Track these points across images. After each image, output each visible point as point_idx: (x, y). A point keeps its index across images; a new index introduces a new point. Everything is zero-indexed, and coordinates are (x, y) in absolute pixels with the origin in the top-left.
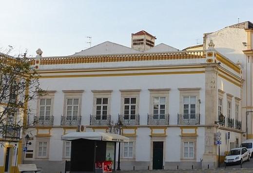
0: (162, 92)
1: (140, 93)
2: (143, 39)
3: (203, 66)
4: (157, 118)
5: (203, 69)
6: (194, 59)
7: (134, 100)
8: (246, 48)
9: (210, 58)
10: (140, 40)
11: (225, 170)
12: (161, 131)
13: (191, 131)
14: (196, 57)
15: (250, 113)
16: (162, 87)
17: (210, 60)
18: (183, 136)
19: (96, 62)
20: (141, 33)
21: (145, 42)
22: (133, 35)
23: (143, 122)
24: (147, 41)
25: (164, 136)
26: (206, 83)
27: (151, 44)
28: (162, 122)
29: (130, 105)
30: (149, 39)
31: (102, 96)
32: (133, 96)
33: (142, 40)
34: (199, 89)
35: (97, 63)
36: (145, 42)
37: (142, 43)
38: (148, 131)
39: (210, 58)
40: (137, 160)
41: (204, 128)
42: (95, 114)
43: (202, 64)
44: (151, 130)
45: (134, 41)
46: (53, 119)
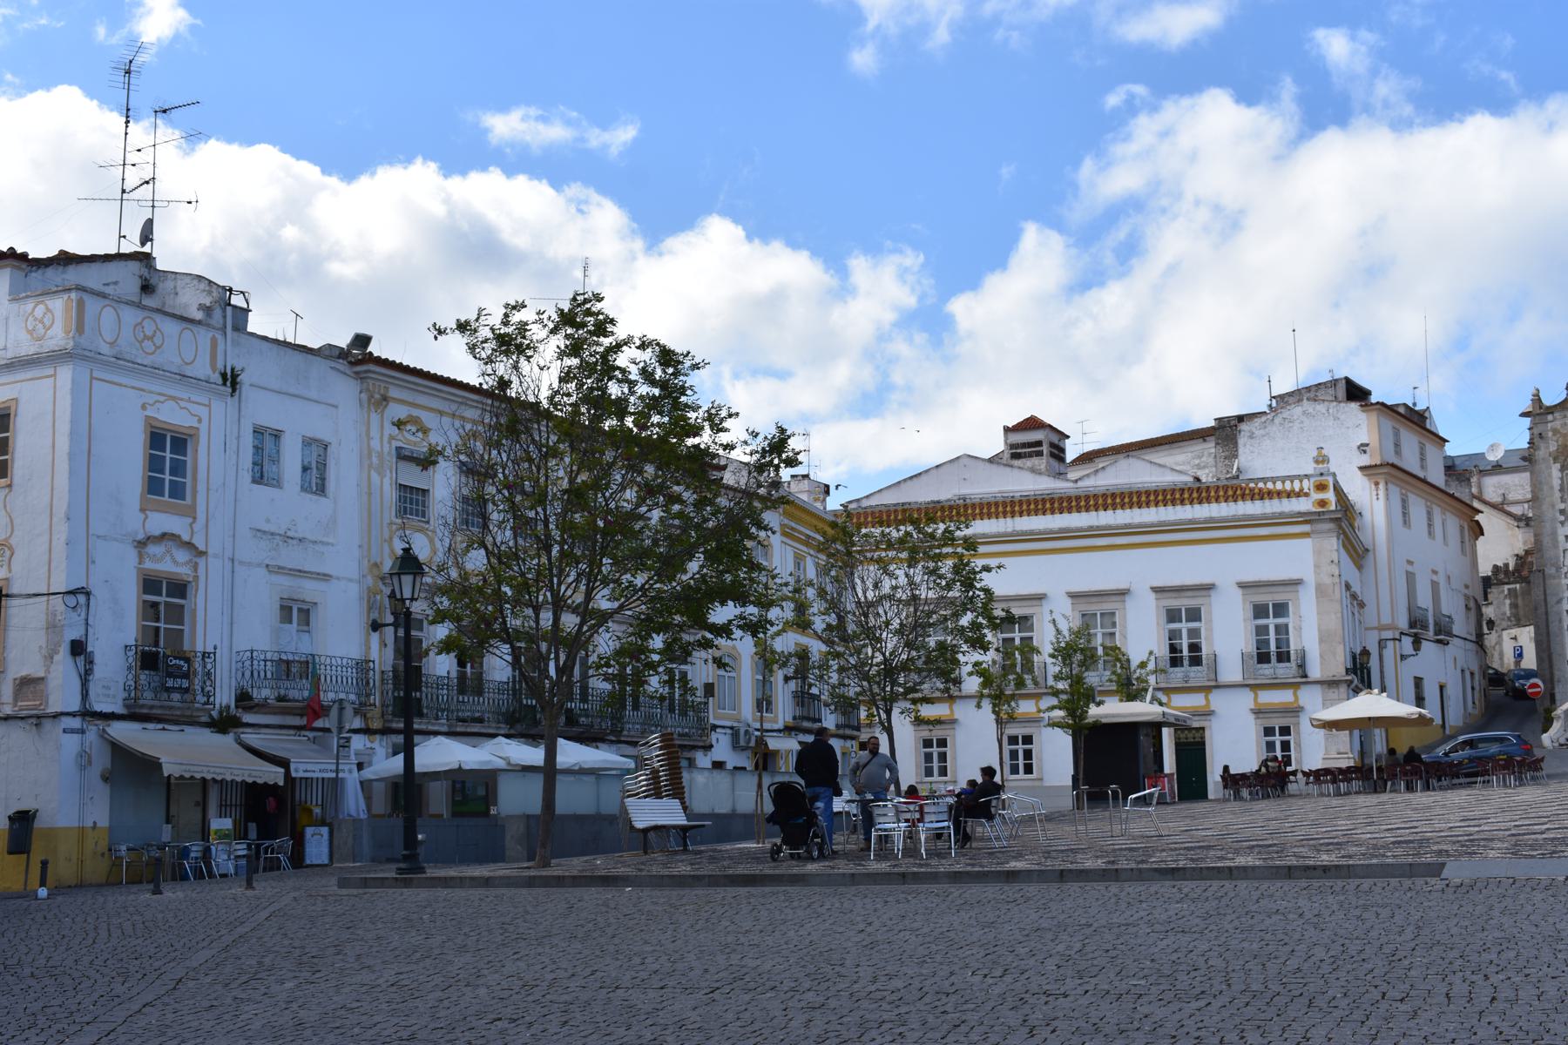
0: (1190, 594)
1: (1127, 598)
2: (1034, 441)
4: (1269, 661)
6: (1276, 501)
7: (1194, 615)
8: (1365, 460)
9: (1321, 496)
10: (1030, 445)
11: (1338, 794)
12: (1282, 697)
13: (1282, 697)
14: (1279, 494)
15: (1390, 644)
16: (1189, 581)
17: (1322, 503)
18: (1258, 712)
19: (1148, 505)
20: (1032, 424)
22: (1007, 430)
23: (1231, 671)
25: (1208, 714)
26: (1317, 566)
28: (1197, 675)
29: (935, 750)
30: (1055, 439)
31: (1183, 602)
32: (1280, 597)
33: (1039, 443)
34: (1298, 583)
35: (993, 521)
36: (1045, 449)
37: (1040, 454)
38: (1246, 700)
39: (1321, 496)
40: (1047, 783)
41: (1318, 688)
42: (1251, 648)
43: (1300, 514)
44: (1251, 695)
45: (1012, 446)
46: (1303, 658)
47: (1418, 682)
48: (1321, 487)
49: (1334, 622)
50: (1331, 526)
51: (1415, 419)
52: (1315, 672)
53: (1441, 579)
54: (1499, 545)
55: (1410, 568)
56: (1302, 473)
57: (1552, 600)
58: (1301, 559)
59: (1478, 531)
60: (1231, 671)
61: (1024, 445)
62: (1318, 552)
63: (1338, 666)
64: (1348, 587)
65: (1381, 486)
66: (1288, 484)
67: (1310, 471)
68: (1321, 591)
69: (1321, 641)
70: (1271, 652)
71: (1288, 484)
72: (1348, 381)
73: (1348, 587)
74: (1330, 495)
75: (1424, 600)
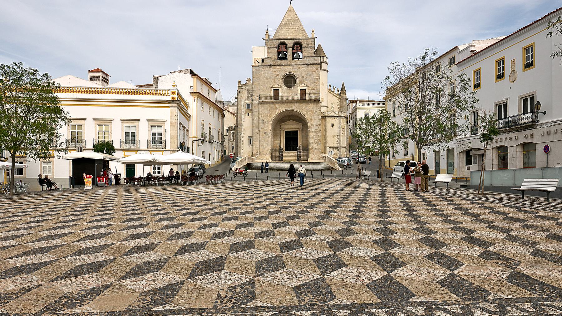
3: (168, 102)
5: (168, 105)
17: (173, 98)
21: (101, 78)
22: (90, 72)
24: (103, 77)
27: (106, 81)
33: (99, 77)
34: (165, 121)
36: (101, 78)
37: (99, 80)
42: (124, 139)
45: (91, 76)
47: (203, 152)
48: (173, 93)
49: (174, 133)
50: (176, 105)
51: (206, 82)
52: (168, 147)
53: (212, 126)
54: (229, 121)
55: (203, 122)
56: (169, 88)
57: (239, 134)
58: (167, 114)
59: (223, 116)
60: (143, 146)
61: (94, 77)
62: (171, 113)
63: (175, 146)
64: (181, 124)
65: (196, 98)
66: (166, 92)
67: (171, 88)
68: (171, 123)
69: (171, 138)
70: (131, 139)
71: (166, 92)
72: (191, 70)
73: (181, 124)
74: (176, 96)
75: (206, 130)
